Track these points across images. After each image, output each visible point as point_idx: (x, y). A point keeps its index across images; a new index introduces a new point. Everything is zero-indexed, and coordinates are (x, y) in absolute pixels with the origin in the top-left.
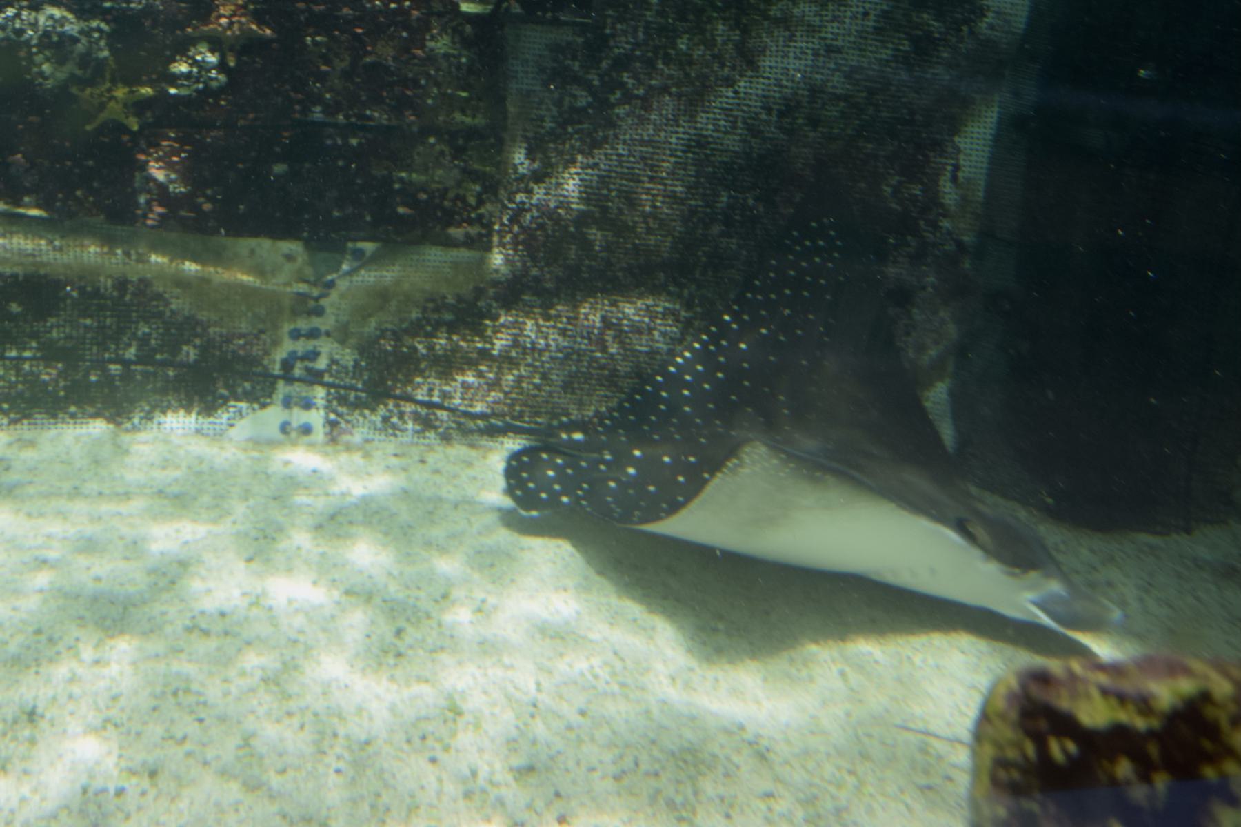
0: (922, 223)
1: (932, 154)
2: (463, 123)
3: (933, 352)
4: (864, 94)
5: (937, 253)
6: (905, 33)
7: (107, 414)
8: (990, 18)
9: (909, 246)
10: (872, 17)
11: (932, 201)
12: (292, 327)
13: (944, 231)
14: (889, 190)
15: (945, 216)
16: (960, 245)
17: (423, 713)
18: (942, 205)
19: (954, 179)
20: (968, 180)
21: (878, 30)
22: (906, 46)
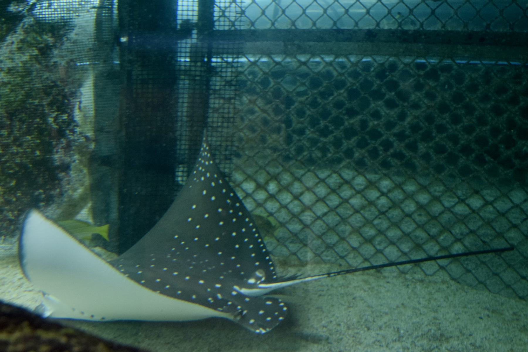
0: (67, 132)
1: (71, 99)
2: (217, 58)
3: (80, 191)
4: (20, 79)
5: (76, 144)
6: (36, 47)
7: (157, 218)
8: (76, 30)
9: (63, 143)
10: (16, 43)
11: (71, 120)
12: (476, 113)
13: (78, 133)
14: (52, 119)
15: (77, 126)
16: (87, 138)
17: (517, 299)
18: (75, 121)
19: (80, 108)
20: (85, 107)
21: (19, 49)
22: (36, 52)
